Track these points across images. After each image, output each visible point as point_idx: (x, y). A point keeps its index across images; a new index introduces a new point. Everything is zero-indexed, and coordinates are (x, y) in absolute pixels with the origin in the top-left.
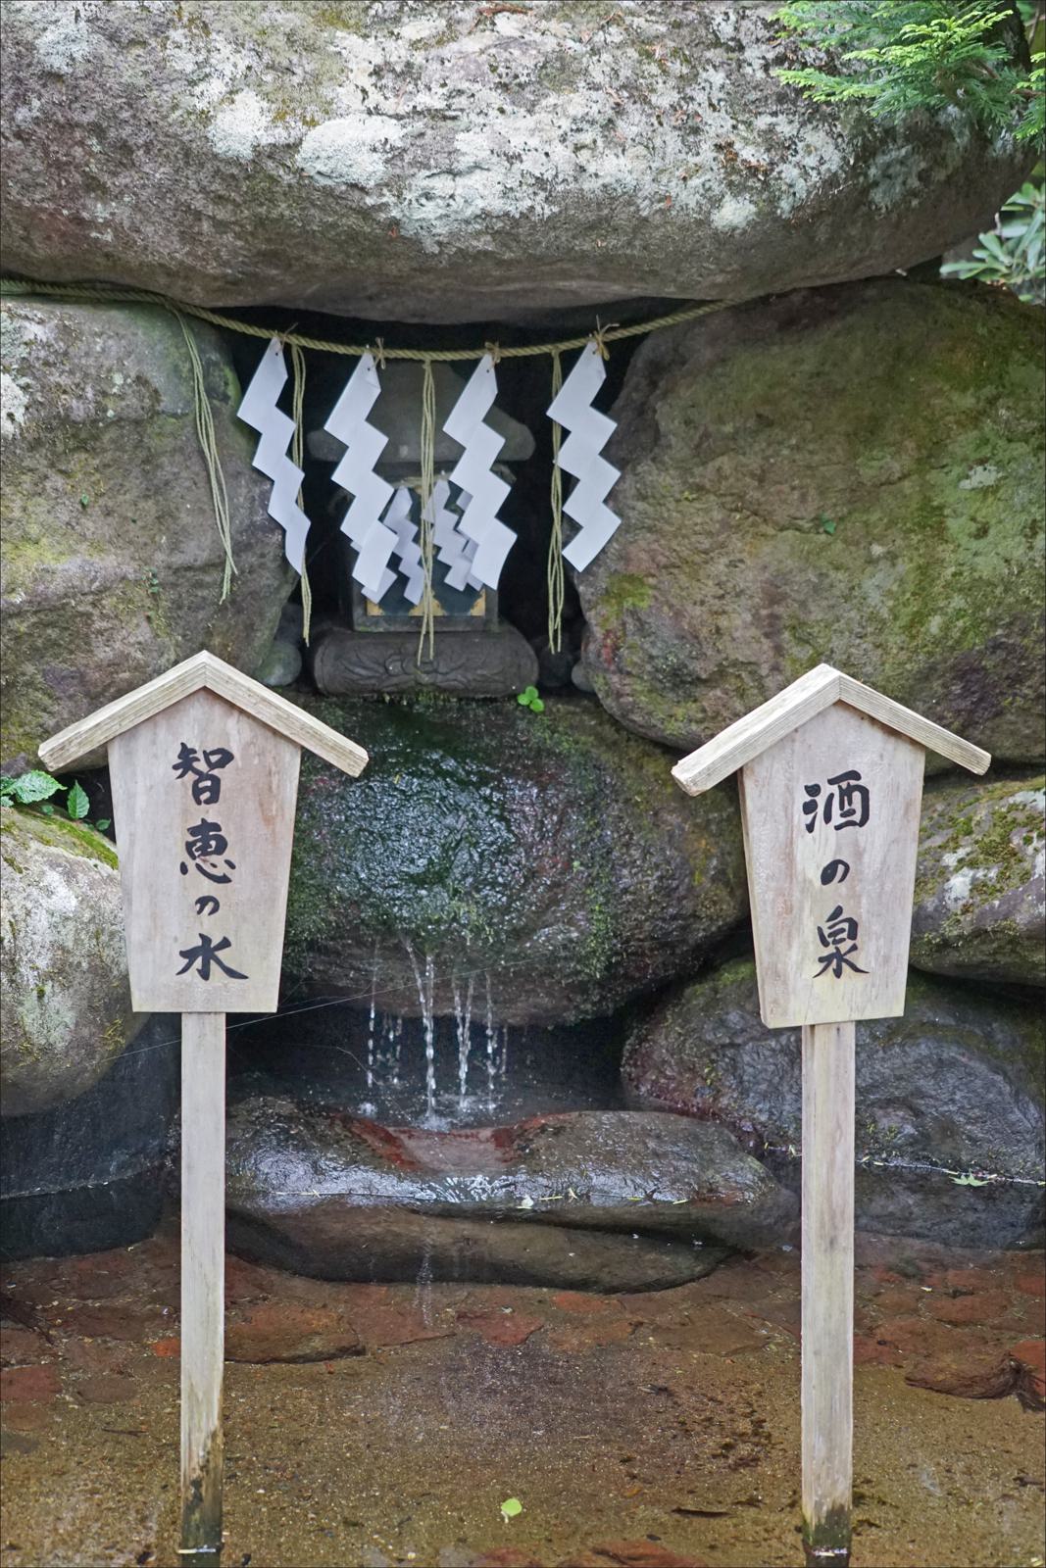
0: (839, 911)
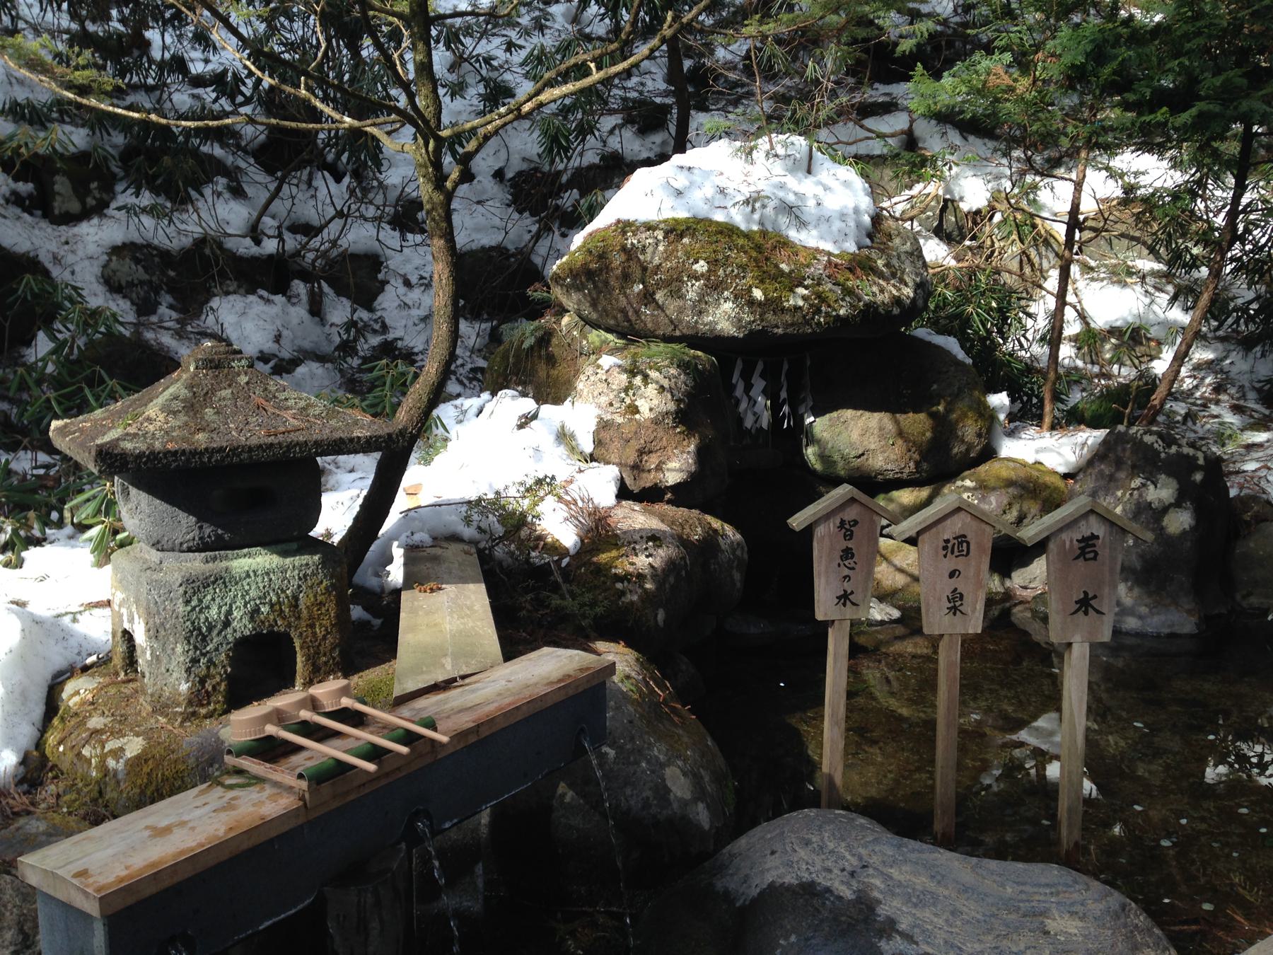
0: (956, 589)
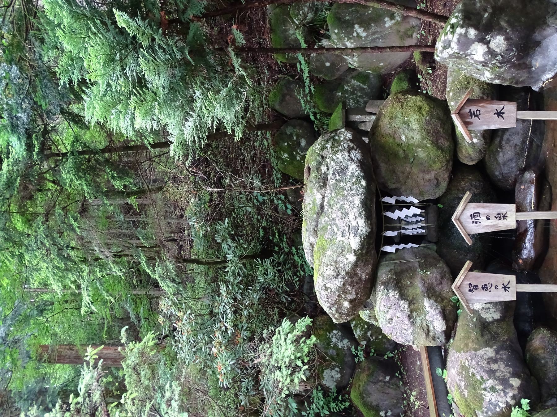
0: (495, 217)
